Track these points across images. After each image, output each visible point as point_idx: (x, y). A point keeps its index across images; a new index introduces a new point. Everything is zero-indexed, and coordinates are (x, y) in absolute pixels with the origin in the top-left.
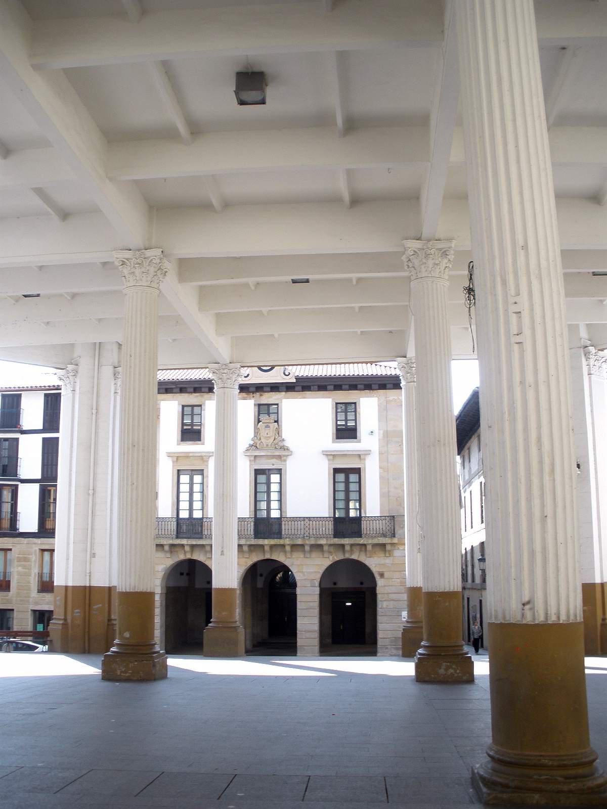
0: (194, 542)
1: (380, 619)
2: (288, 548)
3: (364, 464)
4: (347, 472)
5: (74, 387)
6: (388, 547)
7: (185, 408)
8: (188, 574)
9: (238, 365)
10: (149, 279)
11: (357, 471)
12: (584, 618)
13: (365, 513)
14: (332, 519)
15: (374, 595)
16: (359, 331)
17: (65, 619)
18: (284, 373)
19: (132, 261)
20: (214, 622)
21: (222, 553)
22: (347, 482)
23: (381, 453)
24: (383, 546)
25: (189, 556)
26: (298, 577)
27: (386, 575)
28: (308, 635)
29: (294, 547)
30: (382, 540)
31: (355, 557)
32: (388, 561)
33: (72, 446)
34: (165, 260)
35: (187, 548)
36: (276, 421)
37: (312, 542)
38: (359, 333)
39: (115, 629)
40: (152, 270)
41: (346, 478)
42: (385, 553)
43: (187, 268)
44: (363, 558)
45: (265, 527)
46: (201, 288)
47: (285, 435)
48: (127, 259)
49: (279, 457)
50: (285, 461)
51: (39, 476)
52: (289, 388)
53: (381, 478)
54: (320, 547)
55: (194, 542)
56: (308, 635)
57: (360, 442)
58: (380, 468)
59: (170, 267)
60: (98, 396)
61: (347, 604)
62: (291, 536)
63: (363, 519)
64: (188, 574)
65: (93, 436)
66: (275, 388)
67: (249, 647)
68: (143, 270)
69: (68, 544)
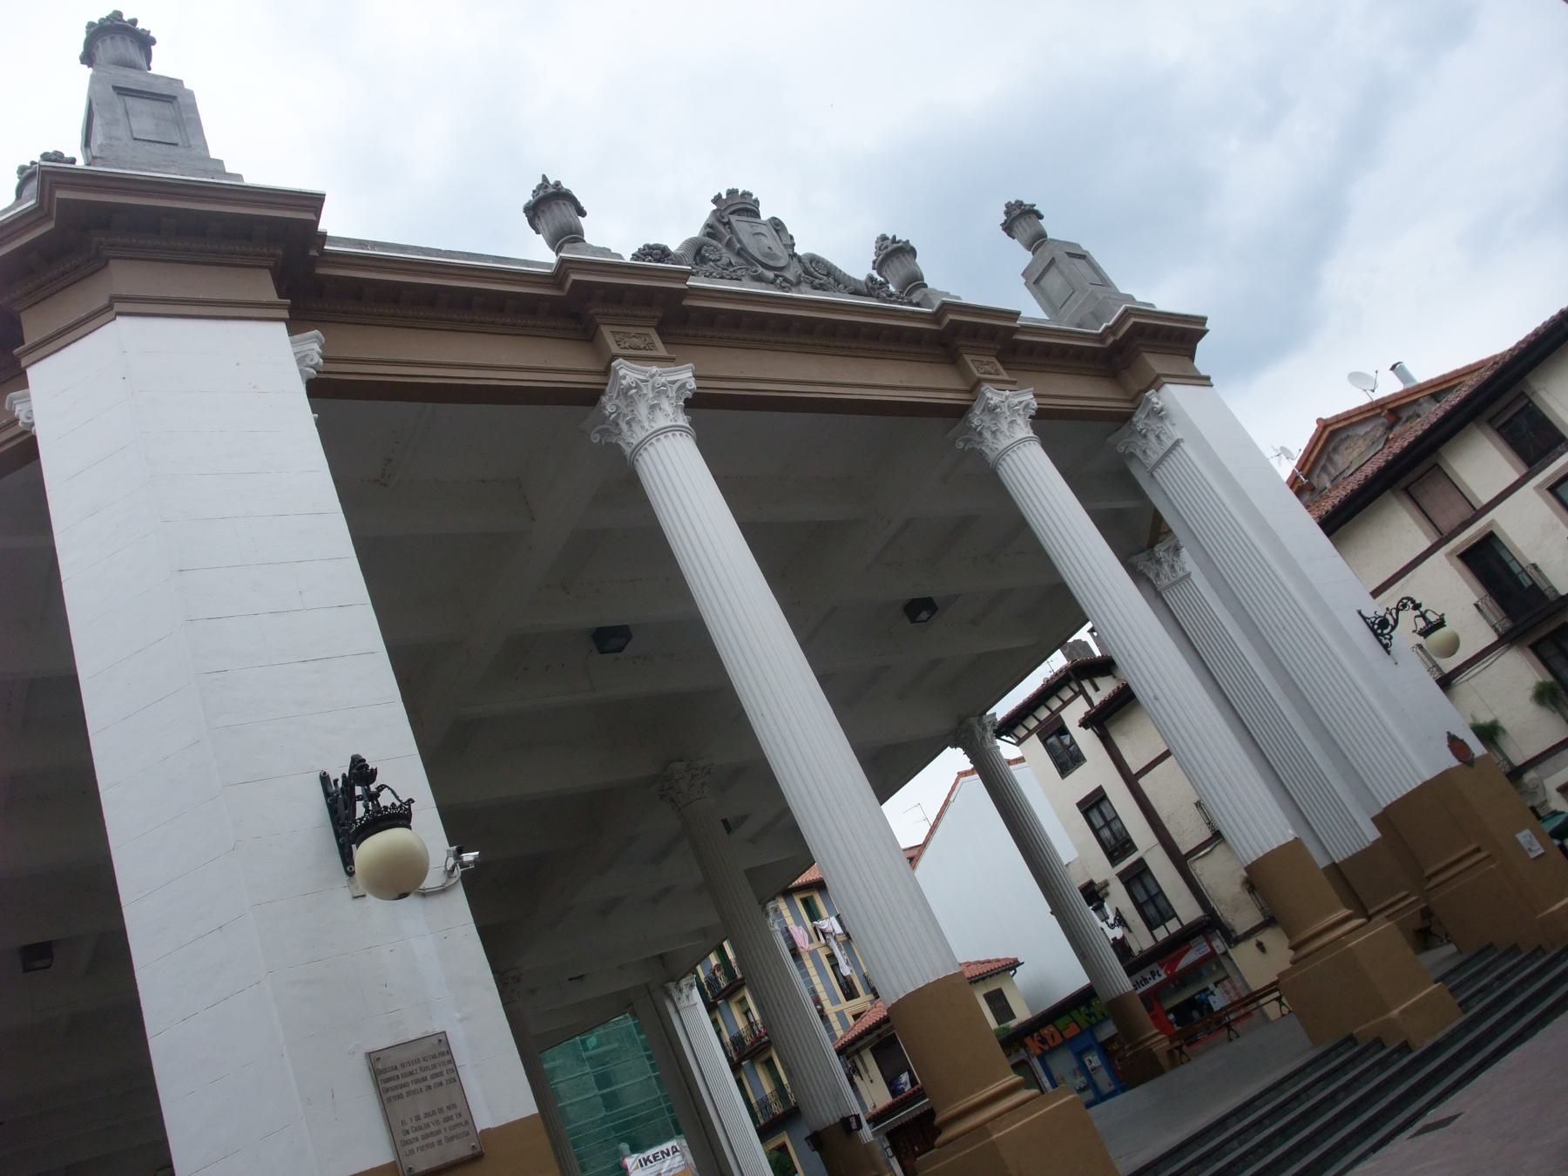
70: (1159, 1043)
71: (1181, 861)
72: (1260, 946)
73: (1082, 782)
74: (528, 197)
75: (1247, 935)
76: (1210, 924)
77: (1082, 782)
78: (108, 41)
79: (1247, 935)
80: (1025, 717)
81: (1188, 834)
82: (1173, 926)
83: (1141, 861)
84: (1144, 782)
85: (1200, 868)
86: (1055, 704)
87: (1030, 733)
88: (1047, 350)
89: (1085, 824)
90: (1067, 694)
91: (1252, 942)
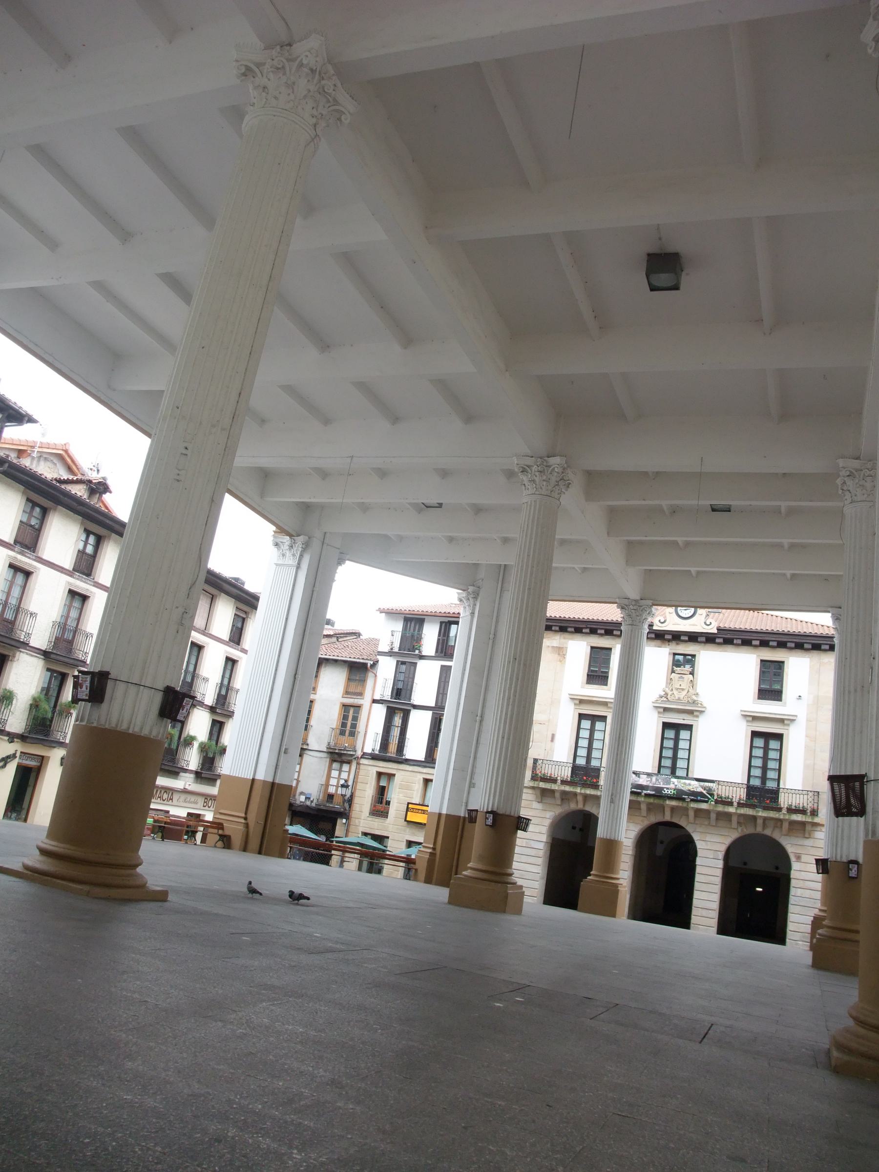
0: (589, 791)
1: (791, 908)
4: (768, 737)
5: (474, 609)
6: (808, 828)
8: (581, 830)
9: (650, 602)
10: (550, 488)
11: (779, 737)
13: (784, 784)
14: (745, 786)
15: (787, 879)
16: (789, 573)
17: (434, 849)
18: (705, 623)
19: (533, 469)
20: (594, 875)
22: (766, 749)
23: (808, 720)
25: (580, 806)
28: (704, 913)
31: (768, 832)
33: (464, 670)
34: (569, 471)
35: (580, 798)
36: (692, 673)
38: (789, 576)
40: (554, 479)
41: (767, 740)
42: (804, 834)
43: (596, 483)
44: (776, 835)
46: (630, 543)
47: (699, 689)
48: (529, 466)
51: (433, 705)
52: (709, 639)
53: (806, 747)
55: (589, 791)
56: (704, 913)
58: (806, 736)
59: (577, 480)
60: (497, 622)
61: (760, 889)
63: (781, 790)
64: (581, 830)
65: (488, 661)
66: (693, 637)
68: (545, 478)
69: (448, 768)
85: (745, 664)
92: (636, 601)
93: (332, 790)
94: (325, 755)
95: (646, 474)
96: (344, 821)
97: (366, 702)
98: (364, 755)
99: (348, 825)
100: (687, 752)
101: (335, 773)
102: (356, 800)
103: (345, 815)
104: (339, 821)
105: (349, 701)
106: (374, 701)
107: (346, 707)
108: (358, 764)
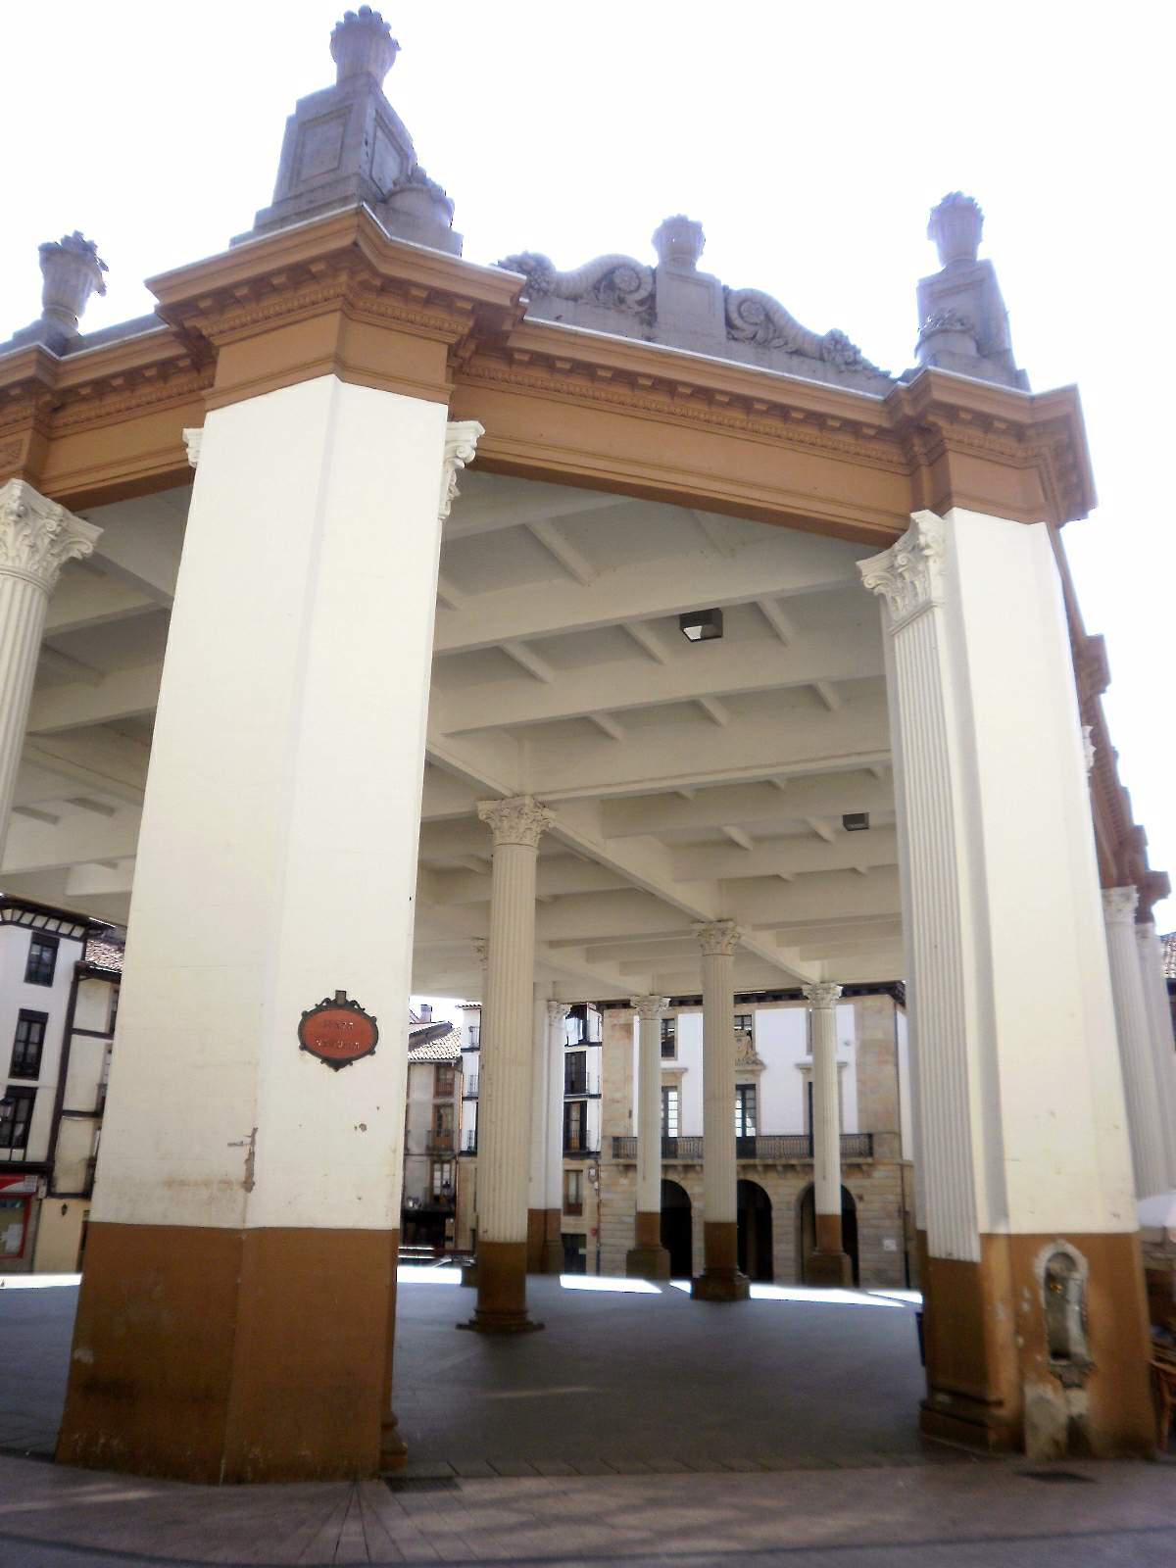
2: (760, 1169)
3: (759, 1081)
6: (865, 1168)
7: (102, 1028)
12: (529, 1237)
21: (644, 1178)
24: (859, 1166)
26: (774, 1199)
27: (866, 1198)
29: (768, 1168)
30: (860, 1160)
32: (866, 1182)
37: (783, 1161)
39: (581, 1251)
45: (669, 1146)
47: (759, 1046)
49: (752, 1072)
50: (759, 1076)
54: (792, 1167)
57: (676, 1060)
62: (763, 1157)
67: (1052, 1272)
70: (250, 1476)
71: (59, 1113)
72: (65, 1208)
73: (37, 998)
74: (56, 237)
75: (63, 1196)
76: (44, 1170)
77: (37, 998)
78: (508, 1235)
79: (63, 1196)
80: (30, 911)
81: (79, 1097)
82: (17, 1154)
83: (14, 1074)
84: (76, 1039)
85: (68, 1126)
86: (65, 929)
87: (29, 926)
88: (133, 378)
89: (15, 1029)
90: (78, 932)
91: (60, 1203)
92: (646, 997)
93: (437, 1191)
94: (425, 1158)
95: (769, 784)
96: (452, 1220)
97: (456, 1099)
98: (462, 1153)
99: (457, 1223)
100: (78, 1024)
101: (437, 1174)
102: (460, 1199)
103: (452, 1214)
104: (447, 1221)
105: (440, 1101)
106: (463, 1099)
107: (437, 1108)
108: (457, 1163)
